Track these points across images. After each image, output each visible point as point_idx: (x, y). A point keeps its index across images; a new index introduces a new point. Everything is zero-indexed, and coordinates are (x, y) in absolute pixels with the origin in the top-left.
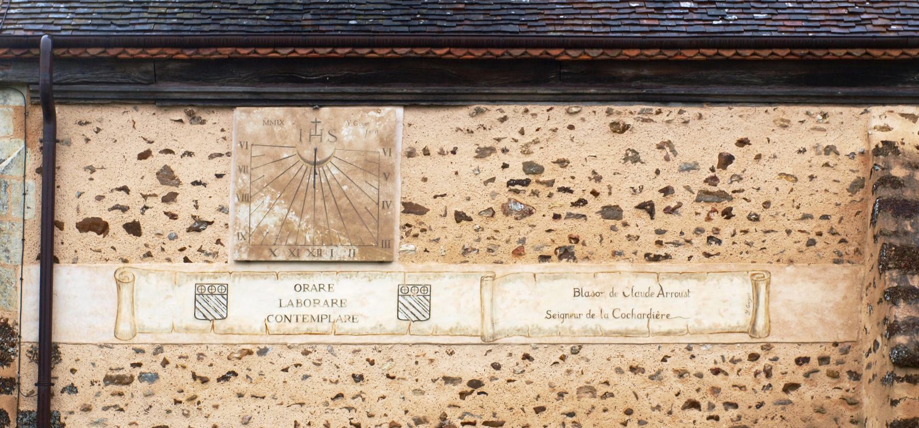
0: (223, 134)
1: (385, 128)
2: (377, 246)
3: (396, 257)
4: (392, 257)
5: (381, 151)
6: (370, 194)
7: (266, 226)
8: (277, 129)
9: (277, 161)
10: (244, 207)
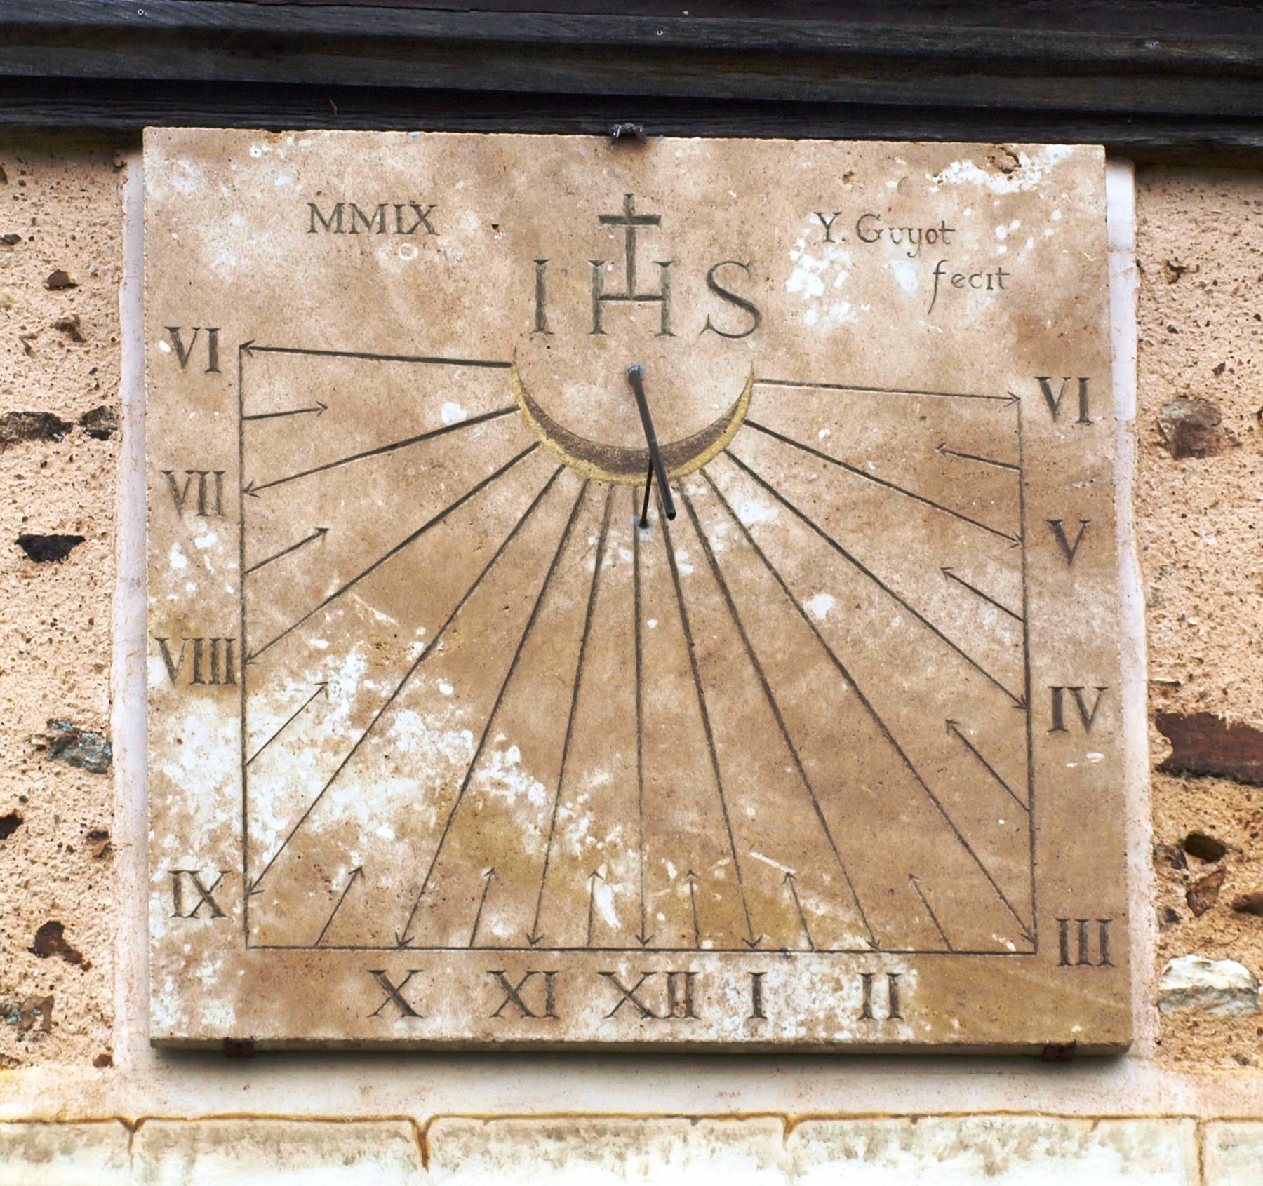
0: (58, 306)
1: (1044, 259)
2: (1030, 955)
3: (1146, 1032)
4: (1125, 1018)
5: (1029, 391)
6: (977, 647)
7: (349, 831)
8: (394, 257)
9: (404, 443)
10: (205, 720)
